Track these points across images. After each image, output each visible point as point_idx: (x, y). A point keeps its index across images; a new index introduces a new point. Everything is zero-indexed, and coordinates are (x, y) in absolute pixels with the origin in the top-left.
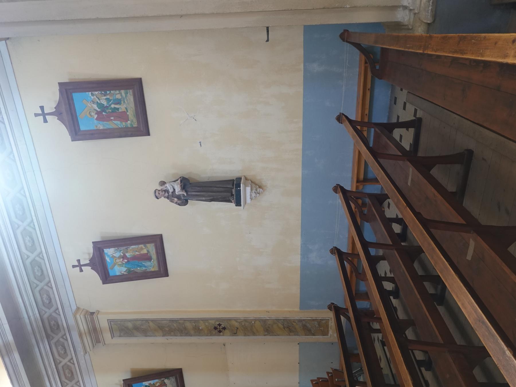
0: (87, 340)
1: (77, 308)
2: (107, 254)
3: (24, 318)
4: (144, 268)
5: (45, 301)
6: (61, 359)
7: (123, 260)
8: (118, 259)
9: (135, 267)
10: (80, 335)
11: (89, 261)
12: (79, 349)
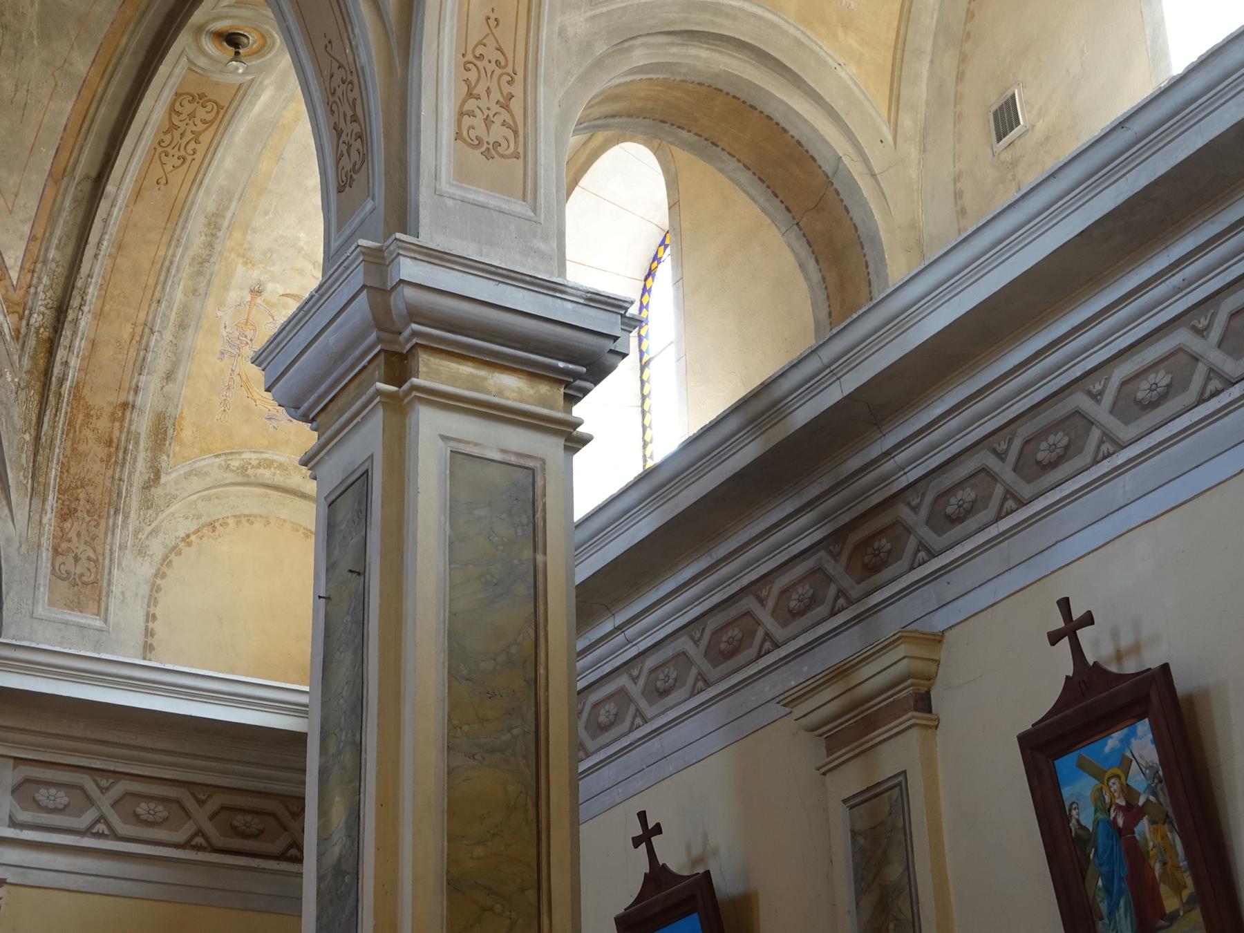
0: (827, 701)
1: (934, 634)
2: (1133, 734)
3: (884, 435)
4: (1104, 907)
5: (953, 500)
6: (771, 603)
7: (1119, 807)
8: (1121, 784)
9: (1101, 865)
10: (841, 672)
11: (1095, 663)
12: (805, 669)
